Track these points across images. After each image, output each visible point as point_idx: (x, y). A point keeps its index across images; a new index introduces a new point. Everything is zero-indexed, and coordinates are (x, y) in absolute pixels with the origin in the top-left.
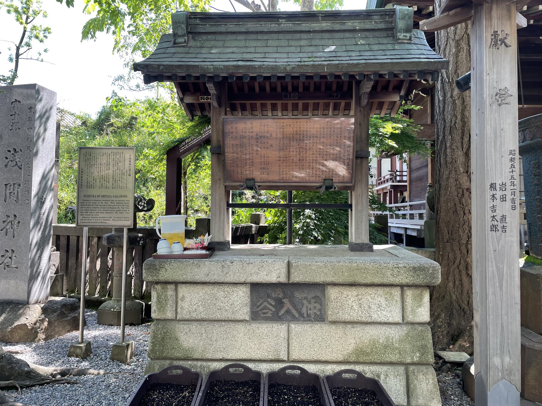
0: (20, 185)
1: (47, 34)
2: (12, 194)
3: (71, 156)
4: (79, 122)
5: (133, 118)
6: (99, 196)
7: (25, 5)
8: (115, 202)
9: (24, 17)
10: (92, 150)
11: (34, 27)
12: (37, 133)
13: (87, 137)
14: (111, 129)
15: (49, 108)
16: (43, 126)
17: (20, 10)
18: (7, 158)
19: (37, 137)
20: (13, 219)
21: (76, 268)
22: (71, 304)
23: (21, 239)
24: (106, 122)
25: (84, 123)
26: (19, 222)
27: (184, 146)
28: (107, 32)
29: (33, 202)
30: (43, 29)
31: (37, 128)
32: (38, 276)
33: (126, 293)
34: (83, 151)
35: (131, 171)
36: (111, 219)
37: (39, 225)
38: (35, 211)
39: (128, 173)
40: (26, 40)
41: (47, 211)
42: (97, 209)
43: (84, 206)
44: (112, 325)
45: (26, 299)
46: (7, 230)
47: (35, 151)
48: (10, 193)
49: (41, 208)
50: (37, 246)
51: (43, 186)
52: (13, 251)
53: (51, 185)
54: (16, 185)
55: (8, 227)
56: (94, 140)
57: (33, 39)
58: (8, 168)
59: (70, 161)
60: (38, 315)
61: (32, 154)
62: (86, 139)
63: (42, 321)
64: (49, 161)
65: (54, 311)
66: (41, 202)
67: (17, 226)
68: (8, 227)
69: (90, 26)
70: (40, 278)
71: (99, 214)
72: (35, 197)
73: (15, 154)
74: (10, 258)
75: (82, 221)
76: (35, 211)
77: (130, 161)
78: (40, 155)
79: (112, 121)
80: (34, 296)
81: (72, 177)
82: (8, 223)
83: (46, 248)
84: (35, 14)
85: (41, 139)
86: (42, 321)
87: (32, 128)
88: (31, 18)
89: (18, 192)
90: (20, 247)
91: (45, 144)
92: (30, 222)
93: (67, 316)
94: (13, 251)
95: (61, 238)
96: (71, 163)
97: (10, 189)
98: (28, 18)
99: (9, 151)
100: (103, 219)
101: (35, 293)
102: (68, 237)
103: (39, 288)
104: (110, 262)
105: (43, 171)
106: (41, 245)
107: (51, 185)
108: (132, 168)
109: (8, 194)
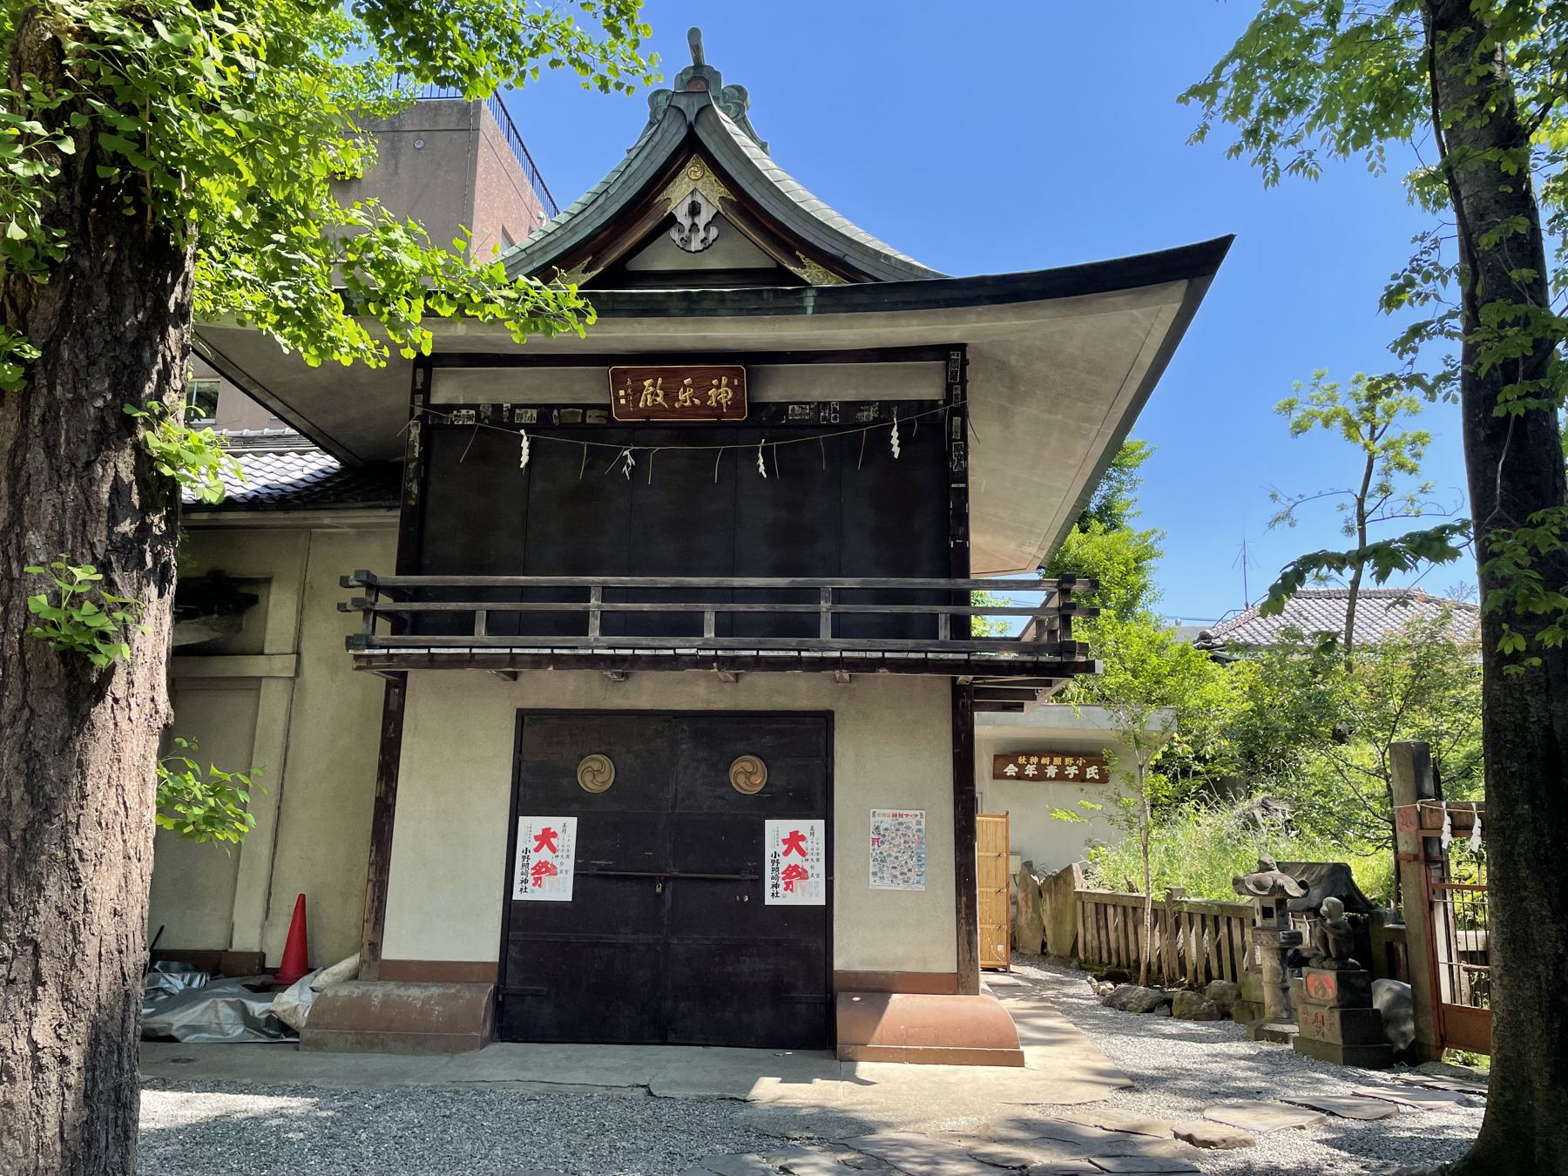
9: (1365, 429)
33: (742, 307)
40: (1375, 480)
57: (1394, 472)
98: (1373, 428)
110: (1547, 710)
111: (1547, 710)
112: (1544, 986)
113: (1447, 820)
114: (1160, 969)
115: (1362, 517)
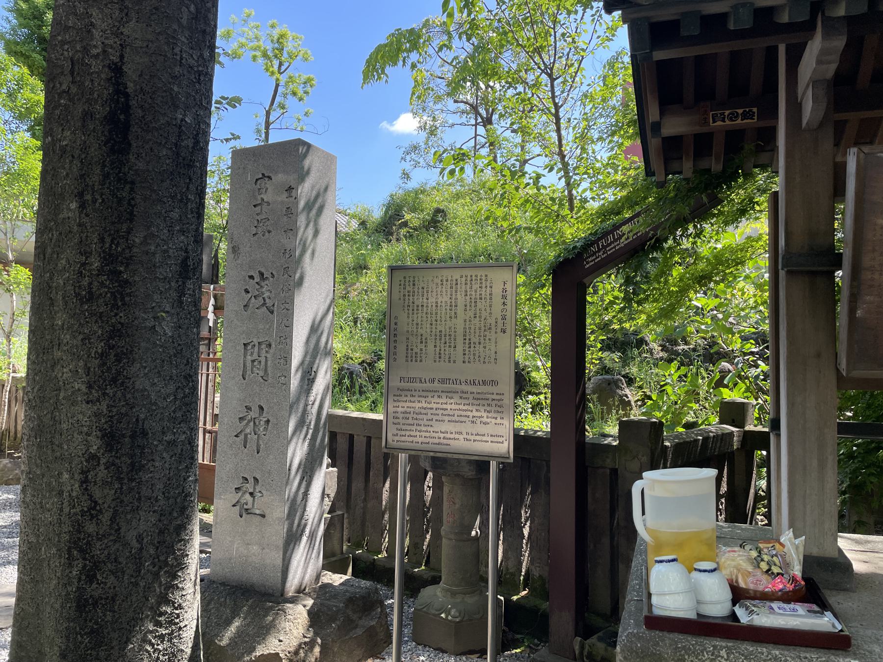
0: (270, 345)
1: (309, 89)
2: (256, 363)
3: (345, 278)
4: (355, 224)
5: (438, 211)
6: (433, 381)
7: (276, 45)
8: (471, 396)
9: (276, 63)
10: (411, 273)
11: (290, 77)
12: (301, 240)
13: (369, 247)
14: (403, 231)
15: (324, 187)
16: (312, 224)
17: (270, 54)
18: (247, 291)
19: (301, 247)
20: (257, 415)
21: (365, 499)
22: (363, 597)
23: (271, 457)
24: (395, 219)
25: (363, 223)
26: (268, 421)
27: (595, 253)
28: (404, 65)
29: (295, 382)
30: (303, 80)
31: (302, 230)
32: (301, 535)
34: (399, 275)
35: (508, 321)
36: (461, 437)
37: (305, 428)
38: (298, 400)
39: (500, 325)
40: (278, 99)
41: (319, 397)
42: (430, 412)
43: (401, 404)
44: (444, 651)
45: (279, 585)
46: (246, 435)
47: (298, 275)
48: (253, 361)
49: (308, 391)
50: (301, 471)
51: (312, 346)
52: (256, 480)
53: (327, 343)
54: (263, 346)
55: (248, 431)
56: (378, 251)
57: (289, 96)
58: (249, 312)
59: (343, 287)
60: (301, 631)
61: (292, 283)
62: (367, 250)
63: (311, 644)
64: (324, 295)
65: (333, 619)
66: (308, 379)
67: (266, 429)
68: (248, 431)
69: (377, 57)
70: (305, 539)
71: (433, 423)
72: (297, 371)
73: (263, 284)
74: (251, 494)
75: (396, 438)
76: (298, 400)
77: (504, 297)
78: (306, 284)
79: (407, 217)
80: (294, 578)
81: (349, 314)
82: (249, 421)
83: (317, 474)
84: (291, 57)
85: (309, 252)
86: (311, 644)
87: (292, 230)
88: (286, 65)
89: (266, 361)
90: (269, 473)
91: (316, 260)
92: (288, 422)
93: (356, 627)
94: (256, 480)
95: (338, 437)
96: (346, 289)
97: (252, 354)
98: (281, 64)
99: (251, 277)
100: (442, 435)
101: (296, 572)
102: (351, 437)
103: (304, 558)
104: (429, 493)
105: (312, 317)
106: (309, 469)
107: (327, 343)
108: (508, 314)
109: (249, 364)
110: (118, 34)
111: (118, 34)
112: (66, 510)
113: (212, 301)
114: (16, 433)
115: (268, 124)
